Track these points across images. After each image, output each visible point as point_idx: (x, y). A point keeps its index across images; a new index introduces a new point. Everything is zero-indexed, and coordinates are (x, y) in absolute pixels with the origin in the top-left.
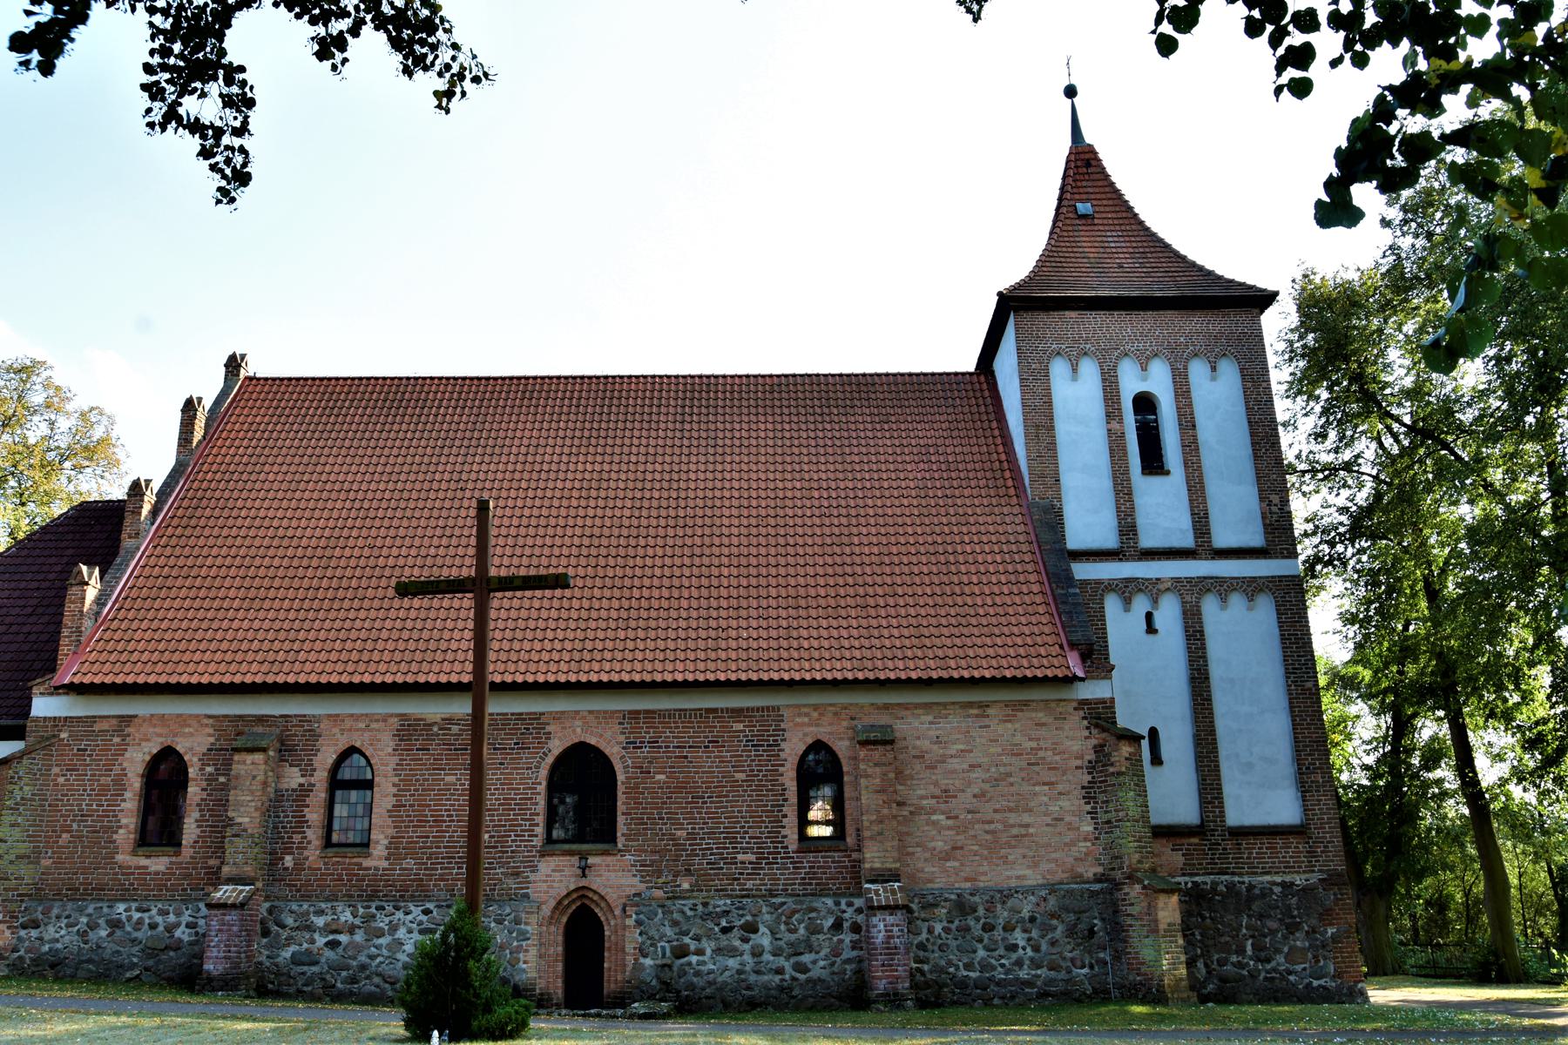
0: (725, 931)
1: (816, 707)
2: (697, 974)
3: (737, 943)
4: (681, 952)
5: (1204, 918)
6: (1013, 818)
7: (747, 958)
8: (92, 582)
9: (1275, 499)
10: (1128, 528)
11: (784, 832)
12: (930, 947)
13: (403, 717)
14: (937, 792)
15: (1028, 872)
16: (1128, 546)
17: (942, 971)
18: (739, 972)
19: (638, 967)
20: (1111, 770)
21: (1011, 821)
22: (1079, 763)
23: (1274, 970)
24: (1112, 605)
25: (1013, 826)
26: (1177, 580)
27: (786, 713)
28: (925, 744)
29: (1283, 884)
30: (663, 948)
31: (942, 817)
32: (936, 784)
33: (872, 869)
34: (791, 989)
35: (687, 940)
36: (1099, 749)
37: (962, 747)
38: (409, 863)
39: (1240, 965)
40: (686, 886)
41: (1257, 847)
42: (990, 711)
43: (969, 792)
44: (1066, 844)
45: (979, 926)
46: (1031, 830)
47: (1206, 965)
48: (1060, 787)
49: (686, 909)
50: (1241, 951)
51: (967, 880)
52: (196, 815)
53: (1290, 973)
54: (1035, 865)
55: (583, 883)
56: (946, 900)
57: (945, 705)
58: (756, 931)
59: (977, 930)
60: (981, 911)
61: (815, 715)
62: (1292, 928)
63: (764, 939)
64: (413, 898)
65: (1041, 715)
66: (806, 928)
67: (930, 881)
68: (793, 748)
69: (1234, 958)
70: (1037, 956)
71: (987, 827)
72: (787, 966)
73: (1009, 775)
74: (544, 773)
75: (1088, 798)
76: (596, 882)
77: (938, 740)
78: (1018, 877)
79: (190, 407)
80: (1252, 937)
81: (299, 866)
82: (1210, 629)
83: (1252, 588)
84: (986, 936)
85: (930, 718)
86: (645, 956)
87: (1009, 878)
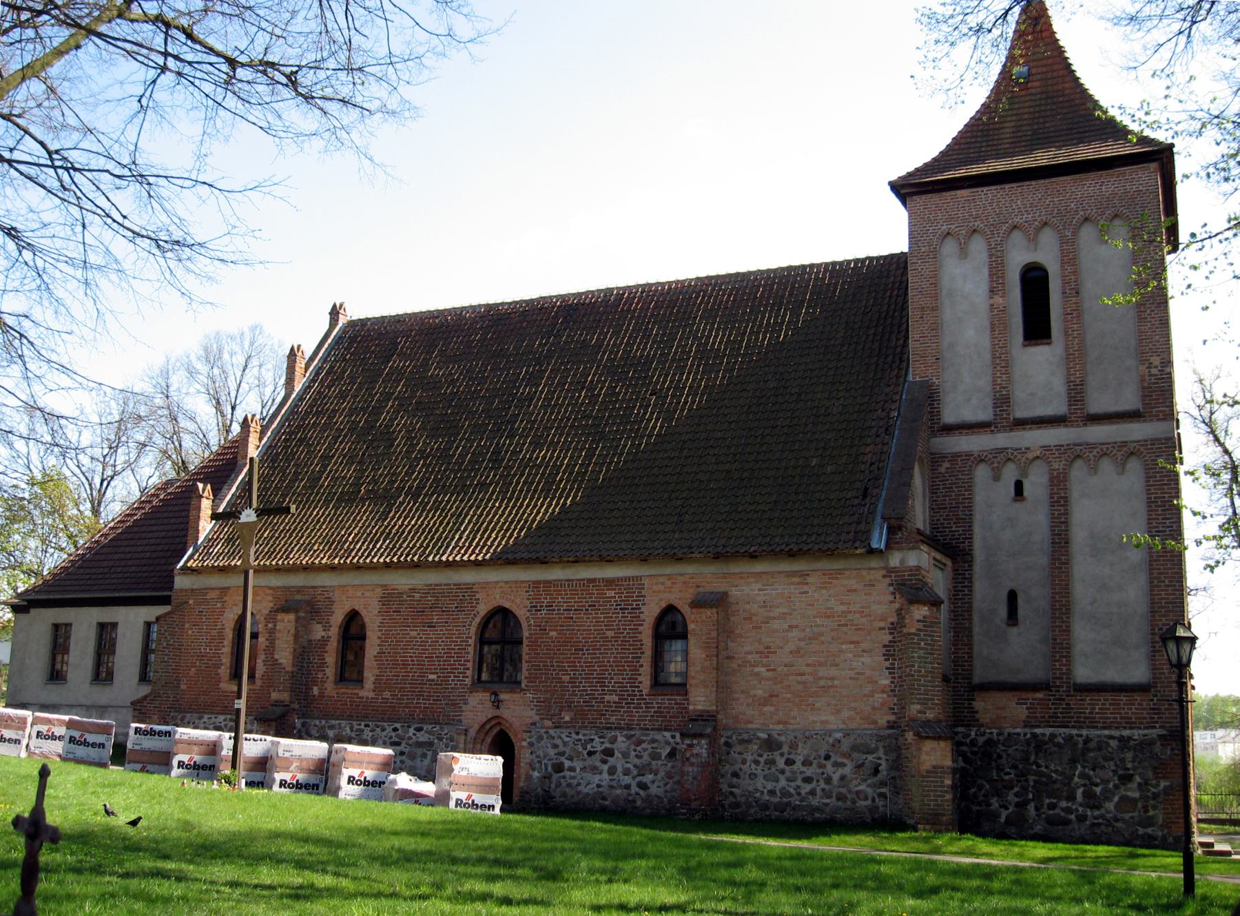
0: (590, 754)
1: (669, 576)
2: (569, 785)
3: (598, 764)
4: (559, 768)
5: (1038, 766)
6: (822, 672)
7: (605, 776)
8: (206, 494)
9: (1156, 361)
10: (1002, 401)
11: (640, 678)
12: (741, 774)
13: (384, 587)
14: (761, 648)
15: (831, 718)
16: (1005, 417)
17: (785, 793)
18: (599, 786)
19: (529, 777)
20: (905, 631)
21: (820, 674)
22: (882, 624)
23: (1102, 816)
24: (982, 473)
25: (821, 678)
26: (1046, 448)
27: (646, 582)
28: (754, 608)
29: (1121, 739)
30: (546, 765)
31: (763, 669)
32: (760, 642)
33: (695, 711)
34: (634, 801)
35: (563, 759)
36: (899, 612)
37: (785, 610)
38: (387, 694)
39: (1068, 810)
40: (567, 718)
41: (1099, 705)
42: (809, 580)
43: (787, 649)
44: (865, 695)
45: (783, 760)
46: (836, 682)
47: (1037, 809)
48: (865, 645)
49: (563, 736)
50: (1071, 797)
51: (779, 723)
52: (263, 657)
53: (1117, 820)
54: (838, 712)
55: (497, 713)
56: (758, 738)
57: (773, 574)
58: (612, 755)
59: (781, 763)
60: (785, 749)
61: (669, 583)
62: (1126, 779)
63: (617, 761)
64: (389, 720)
65: (853, 582)
66: (650, 755)
67: (750, 722)
68: (650, 611)
69: (1064, 804)
70: (826, 787)
71: (799, 678)
72: (634, 785)
73: (821, 634)
74: (473, 629)
75: (887, 656)
76: (505, 713)
77: (764, 605)
78: (822, 722)
79: (292, 355)
80: (1084, 785)
81: (321, 695)
82: (1075, 492)
83: (1126, 452)
84: (787, 768)
85: (759, 586)
86: (534, 769)
87: (815, 722)
